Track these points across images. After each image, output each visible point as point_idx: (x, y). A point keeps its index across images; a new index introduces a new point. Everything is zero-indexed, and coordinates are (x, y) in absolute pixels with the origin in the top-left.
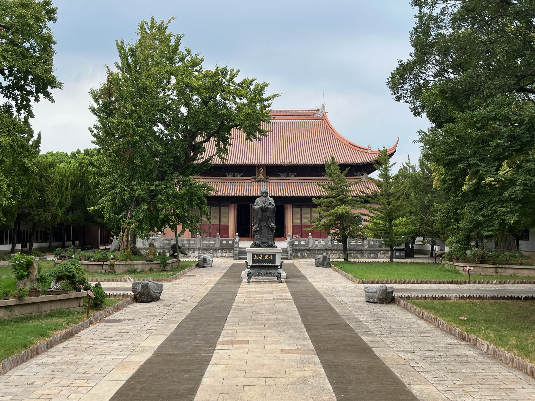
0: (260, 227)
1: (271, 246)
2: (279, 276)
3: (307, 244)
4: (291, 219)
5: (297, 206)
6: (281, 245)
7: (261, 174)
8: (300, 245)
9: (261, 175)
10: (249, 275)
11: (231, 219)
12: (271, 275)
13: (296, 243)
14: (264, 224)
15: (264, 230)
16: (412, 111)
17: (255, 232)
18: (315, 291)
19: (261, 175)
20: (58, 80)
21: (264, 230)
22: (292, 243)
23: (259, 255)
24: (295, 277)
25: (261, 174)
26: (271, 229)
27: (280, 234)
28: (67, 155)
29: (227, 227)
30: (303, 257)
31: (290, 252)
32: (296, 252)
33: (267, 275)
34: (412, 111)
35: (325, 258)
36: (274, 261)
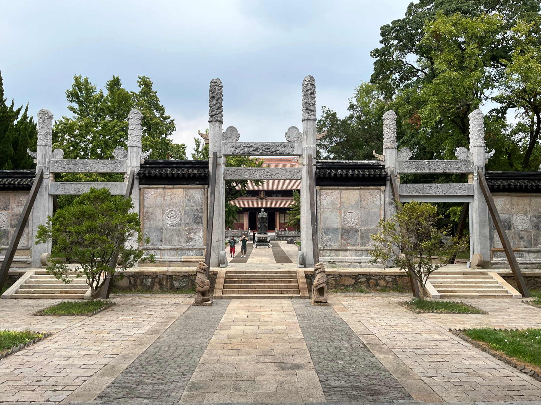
0: (261, 226)
1: (266, 234)
2: (268, 246)
3: (285, 234)
4: (278, 220)
5: (282, 213)
6: (270, 234)
7: (262, 195)
8: (282, 234)
9: (262, 196)
10: (257, 245)
11: (245, 221)
12: (265, 245)
13: (280, 233)
14: (262, 224)
15: (263, 226)
16: (132, 204)
17: (259, 228)
18: (283, 251)
19: (262, 196)
20: (111, 79)
21: (263, 226)
22: (277, 233)
23: (260, 237)
24: (275, 246)
25: (262, 195)
26: (266, 227)
27: (272, 228)
28: (388, 25)
29: (243, 225)
30: (283, 240)
31: (276, 238)
32: (280, 237)
33: (264, 245)
34: (132, 204)
35: (292, 240)
36: (267, 240)
